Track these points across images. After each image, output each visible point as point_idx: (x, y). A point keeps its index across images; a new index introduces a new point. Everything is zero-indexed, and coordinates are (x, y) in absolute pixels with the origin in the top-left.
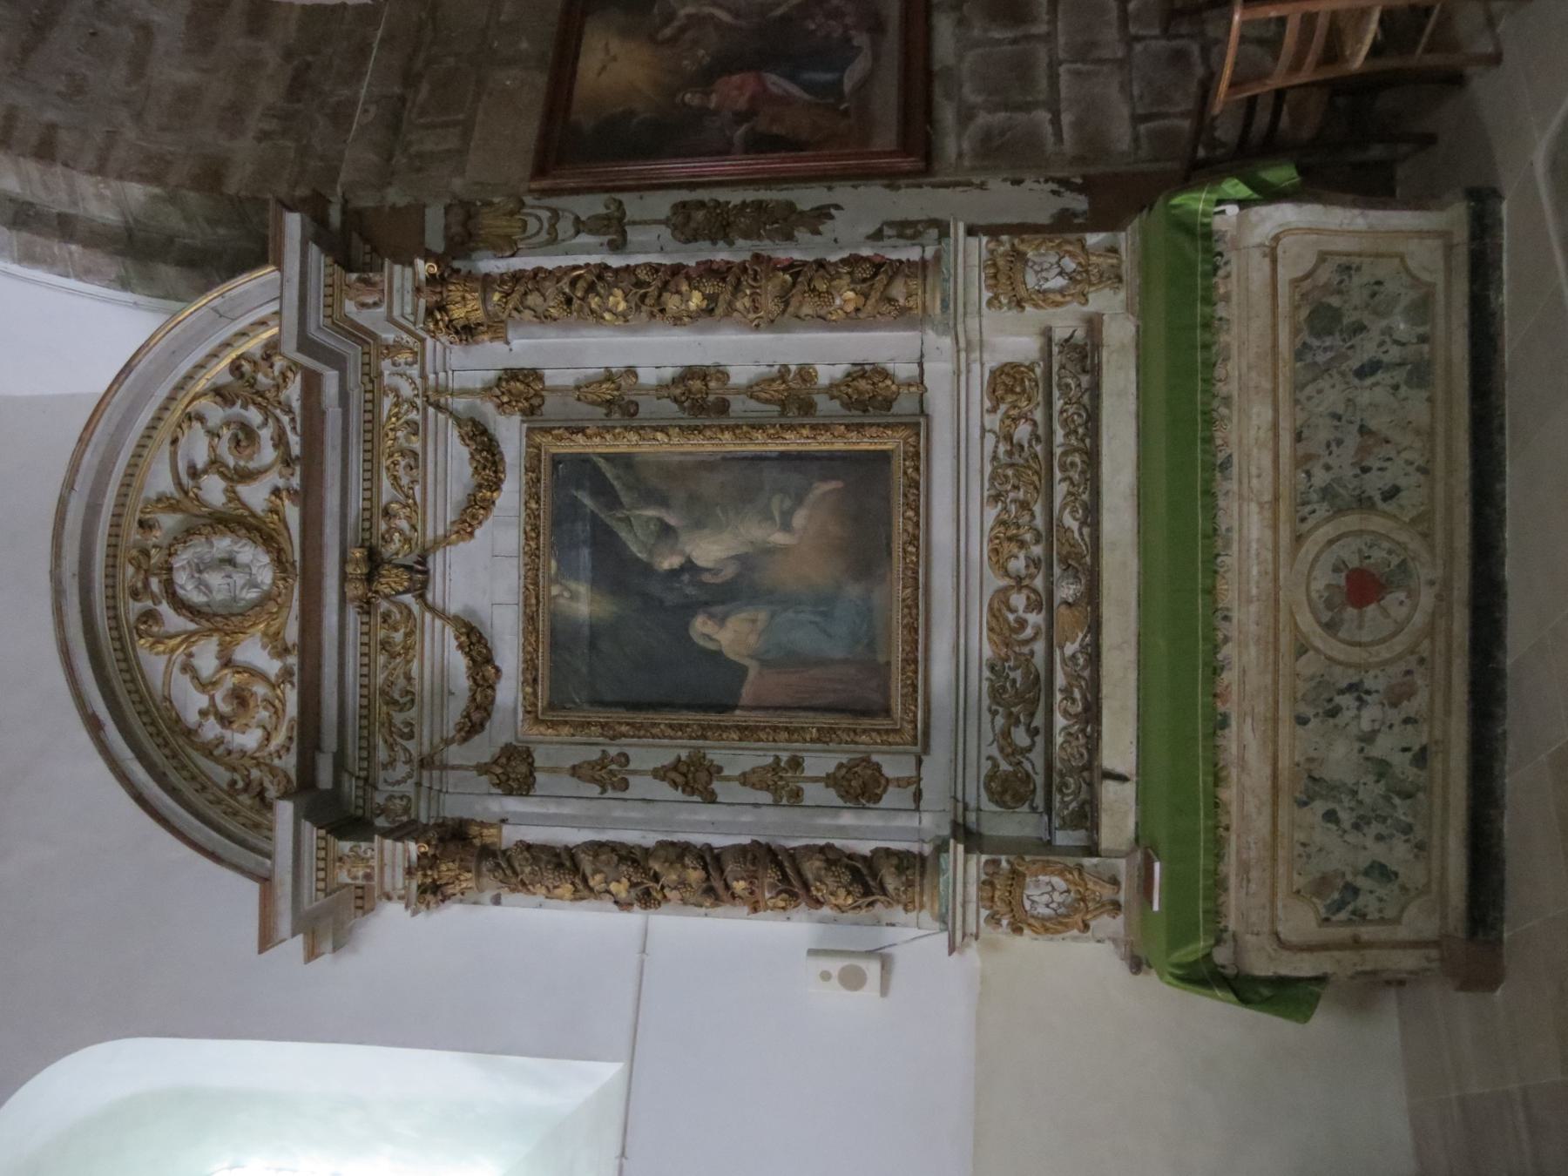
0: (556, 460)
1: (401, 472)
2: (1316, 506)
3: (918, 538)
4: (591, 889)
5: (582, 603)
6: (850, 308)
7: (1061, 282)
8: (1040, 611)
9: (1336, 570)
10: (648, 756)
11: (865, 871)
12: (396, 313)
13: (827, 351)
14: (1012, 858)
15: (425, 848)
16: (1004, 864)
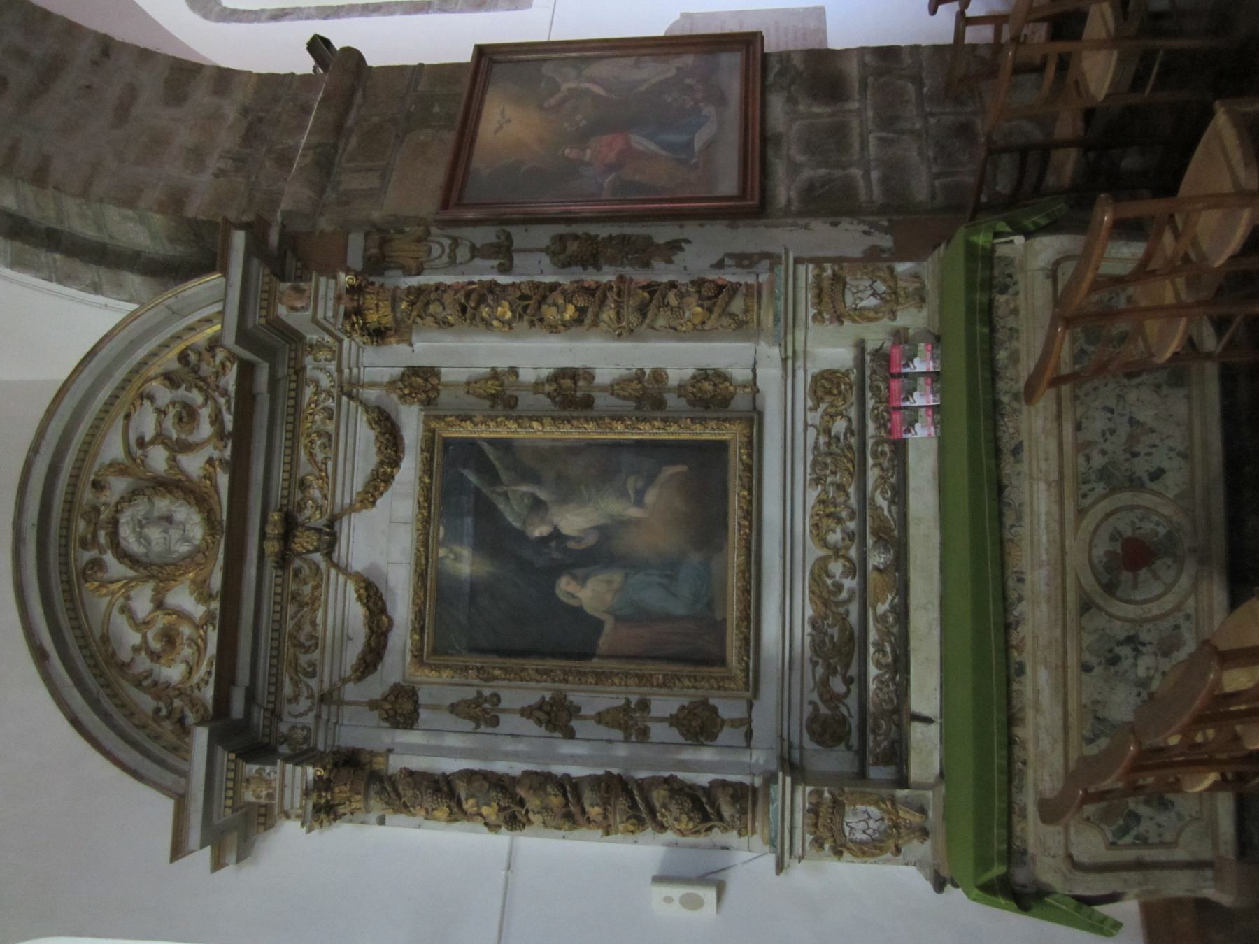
0: (447, 443)
1: (317, 450)
2: (1095, 485)
3: (753, 514)
4: (465, 813)
5: (464, 563)
6: (697, 321)
7: (873, 302)
8: (853, 578)
9: (1113, 538)
10: (517, 696)
11: (704, 800)
12: (320, 316)
13: (677, 357)
14: (833, 789)
15: (321, 772)
16: (827, 795)
